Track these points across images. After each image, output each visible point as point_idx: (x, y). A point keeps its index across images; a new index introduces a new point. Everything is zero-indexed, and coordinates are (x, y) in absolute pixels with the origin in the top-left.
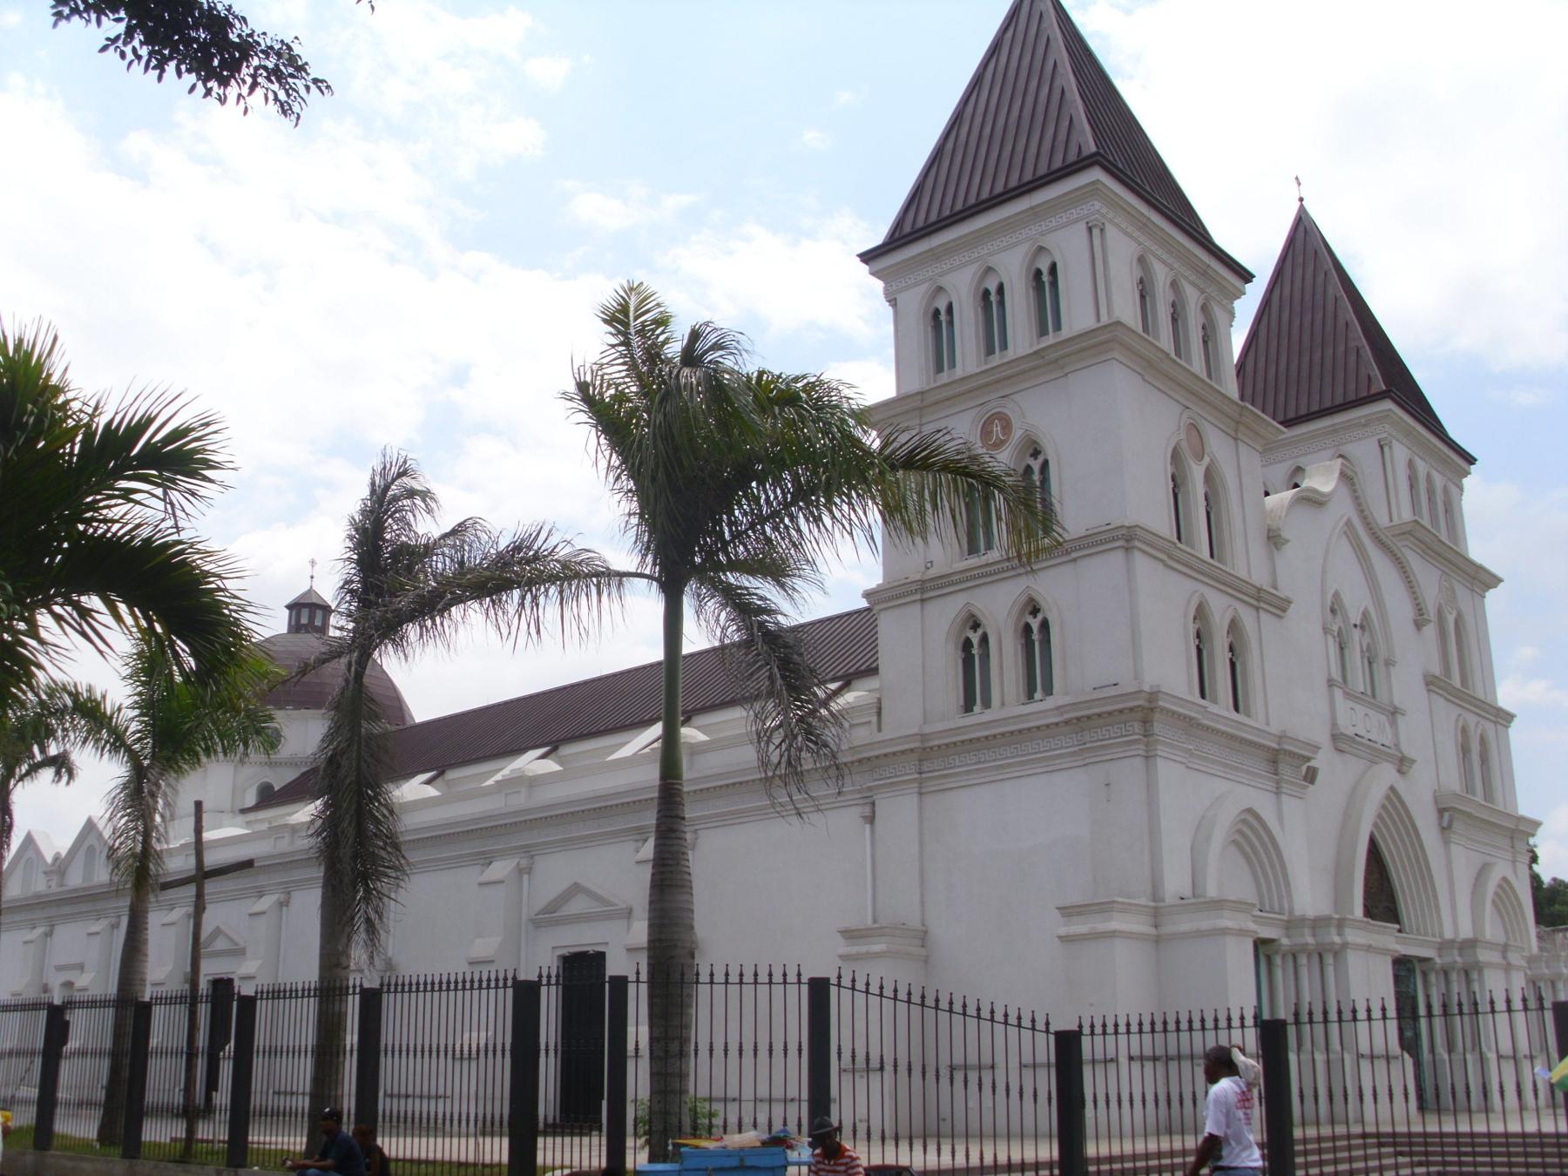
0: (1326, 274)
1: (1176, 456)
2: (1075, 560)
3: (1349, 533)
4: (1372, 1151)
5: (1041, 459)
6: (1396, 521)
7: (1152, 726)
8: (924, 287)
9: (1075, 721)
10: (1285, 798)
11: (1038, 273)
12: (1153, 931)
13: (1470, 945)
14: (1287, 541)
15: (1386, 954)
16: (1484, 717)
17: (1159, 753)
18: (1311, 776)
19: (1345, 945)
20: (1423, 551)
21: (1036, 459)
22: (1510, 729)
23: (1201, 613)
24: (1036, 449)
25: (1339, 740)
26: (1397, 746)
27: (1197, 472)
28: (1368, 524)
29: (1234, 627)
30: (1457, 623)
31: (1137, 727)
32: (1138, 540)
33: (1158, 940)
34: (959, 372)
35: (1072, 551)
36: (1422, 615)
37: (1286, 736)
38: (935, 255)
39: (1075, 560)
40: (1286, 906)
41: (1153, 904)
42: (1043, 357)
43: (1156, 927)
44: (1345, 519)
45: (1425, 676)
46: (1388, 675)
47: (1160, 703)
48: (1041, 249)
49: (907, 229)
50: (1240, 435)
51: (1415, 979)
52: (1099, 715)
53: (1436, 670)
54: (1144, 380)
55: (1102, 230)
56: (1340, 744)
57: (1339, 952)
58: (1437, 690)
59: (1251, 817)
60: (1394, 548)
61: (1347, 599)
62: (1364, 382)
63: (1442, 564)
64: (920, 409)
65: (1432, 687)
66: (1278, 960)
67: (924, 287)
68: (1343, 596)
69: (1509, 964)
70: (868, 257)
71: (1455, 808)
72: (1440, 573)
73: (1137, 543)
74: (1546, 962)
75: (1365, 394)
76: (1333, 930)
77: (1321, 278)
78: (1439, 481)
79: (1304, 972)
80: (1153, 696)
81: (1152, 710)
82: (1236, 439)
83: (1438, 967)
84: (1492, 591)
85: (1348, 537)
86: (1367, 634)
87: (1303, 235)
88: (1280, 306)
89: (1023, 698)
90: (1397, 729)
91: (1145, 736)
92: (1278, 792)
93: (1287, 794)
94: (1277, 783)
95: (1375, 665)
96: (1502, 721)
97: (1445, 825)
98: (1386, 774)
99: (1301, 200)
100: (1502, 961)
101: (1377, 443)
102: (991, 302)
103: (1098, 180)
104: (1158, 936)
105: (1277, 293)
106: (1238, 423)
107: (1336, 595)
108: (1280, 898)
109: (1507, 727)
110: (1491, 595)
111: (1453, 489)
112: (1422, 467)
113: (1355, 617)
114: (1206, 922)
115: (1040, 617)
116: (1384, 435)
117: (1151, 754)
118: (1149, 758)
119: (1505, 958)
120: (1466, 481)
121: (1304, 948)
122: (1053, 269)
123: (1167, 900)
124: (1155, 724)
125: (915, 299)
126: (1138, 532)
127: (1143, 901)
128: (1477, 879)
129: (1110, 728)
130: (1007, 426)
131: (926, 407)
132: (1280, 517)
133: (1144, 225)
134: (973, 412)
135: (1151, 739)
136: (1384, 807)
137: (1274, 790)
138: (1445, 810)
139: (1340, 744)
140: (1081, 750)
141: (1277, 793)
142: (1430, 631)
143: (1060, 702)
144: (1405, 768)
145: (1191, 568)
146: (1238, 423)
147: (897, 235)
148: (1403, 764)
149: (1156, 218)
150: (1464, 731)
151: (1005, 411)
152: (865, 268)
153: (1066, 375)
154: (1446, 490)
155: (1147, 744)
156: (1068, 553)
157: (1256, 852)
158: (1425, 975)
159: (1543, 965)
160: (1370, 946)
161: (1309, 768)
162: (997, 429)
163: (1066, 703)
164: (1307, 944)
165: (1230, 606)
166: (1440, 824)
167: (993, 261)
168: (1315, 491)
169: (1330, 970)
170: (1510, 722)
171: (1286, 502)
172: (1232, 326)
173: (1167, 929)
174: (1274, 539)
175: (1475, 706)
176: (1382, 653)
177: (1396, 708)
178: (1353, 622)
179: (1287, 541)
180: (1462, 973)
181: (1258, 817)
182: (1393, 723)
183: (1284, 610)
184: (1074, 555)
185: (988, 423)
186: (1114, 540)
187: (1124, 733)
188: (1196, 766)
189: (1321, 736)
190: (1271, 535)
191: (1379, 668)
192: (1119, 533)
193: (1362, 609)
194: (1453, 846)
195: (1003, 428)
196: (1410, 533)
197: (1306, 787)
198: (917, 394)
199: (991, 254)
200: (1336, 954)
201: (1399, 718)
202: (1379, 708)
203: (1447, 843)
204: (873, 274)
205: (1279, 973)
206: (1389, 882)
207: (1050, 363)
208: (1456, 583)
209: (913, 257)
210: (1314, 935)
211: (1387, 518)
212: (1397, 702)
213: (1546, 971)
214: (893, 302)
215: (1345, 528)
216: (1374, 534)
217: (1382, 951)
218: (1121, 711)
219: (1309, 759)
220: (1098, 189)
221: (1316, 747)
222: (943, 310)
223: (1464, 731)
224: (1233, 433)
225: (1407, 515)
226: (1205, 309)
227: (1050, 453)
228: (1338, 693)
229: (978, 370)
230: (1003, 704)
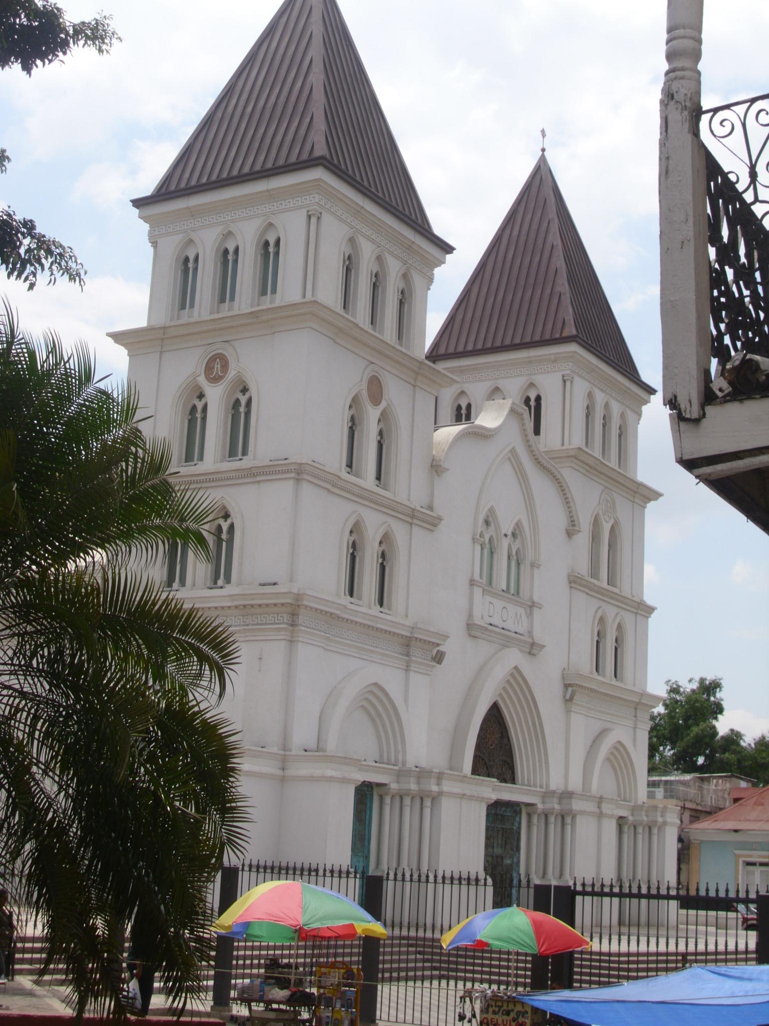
0: (549, 223)
1: (355, 402)
2: (259, 482)
4: (404, 949)
9: (242, 607)
10: (412, 674)
11: (267, 244)
12: (279, 772)
13: (567, 795)
14: (447, 470)
15: (481, 801)
16: (623, 608)
18: (439, 658)
19: (440, 794)
21: (244, 394)
22: (650, 619)
23: (356, 529)
24: (245, 387)
25: (472, 629)
26: (530, 633)
27: (372, 414)
29: (386, 539)
30: (613, 529)
31: (286, 618)
33: (283, 780)
37: (417, 628)
38: (192, 213)
39: (259, 482)
40: (400, 759)
41: (282, 752)
42: (257, 317)
43: (283, 769)
44: (510, 448)
45: (569, 576)
47: (305, 603)
48: (271, 225)
50: (418, 383)
51: (520, 819)
52: (260, 605)
53: (583, 569)
54: (334, 342)
56: (473, 632)
57: (436, 799)
58: (578, 587)
59: (376, 691)
65: (573, 585)
66: (388, 800)
69: (601, 813)
70: (138, 203)
71: (577, 685)
73: (306, 477)
74: (647, 811)
75: (558, 336)
76: (433, 781)
80: (299, 597)
81: (299, 606)
82: (414, 386)
83: (539, 811)
84: (652, 503)
85: (511, 462)
86: (518, 541)
87: (538, 183)
88: (508, 245)
89: (209, 583)
92: (407, 670)
95: (522, 567)
97: (568, 697)
98: (514, 657)
99: (543, 150)
100: (597, 810)
102: (228, 260)
105: (508, 232)
106: (417, 373)
107: (491, 510)
108: (396, 751)
109: (648, 617)
111: (630, 415)
112: (600, 398)
113: (507, 527)
116: (568, 372)
118: (291, 642)
119: (599, 807)
121: (408, 793)
122: (278, 242)
124: (301, 617)
125: (172, 244)
127: (274, 749)
128: (594, 741)
129: (267, 616)
130: (225, 366)
131: (166, 338)
132: (444, 451)
133: (358, 212)
135: (296, 628)
137: (405, 667)
138: (570, 685)
139: (473, 632)
140: (244, 629)
141: (406, 670)
142: (583, 539)
143: (232, 592)
144: (534, 651)
146: (417, 373)
147: (163, 191)
148: (532, 649)
149: (369, 206)
150: (602, 621)
151: (225, 353)
153: (274, 333)
154: (623, 416)
157: (379, 715)
158: (529, 816)
159: (644, 813)
160: (464, 795)
161: (438, 651)
162: (217, 366)
165: (385, 523)
168: (482, 428)
169: (427, 812)
170: (651, 613)
173: (291, 772)
174: (436, 468)
176: (530, 555)
177: (533, 602)
178: (504, 532)
179: (447, 470)
180: (560, 818)
181: (382, 690)
182: (530, 615)
183: (435, 526)
184: (258, 478)
186: (288, 472)
188: (334, 649)
190: (434, 463)
191: (525, 568)
192: (292, 467)
193: (515, 521)
194: (573, 715)
195: (222, 366)
196: (575, 457)
198: (161, 328)
199: (233, 221)
201: (536, 611)
203: (568, 712)
204: (140, 217)
205: (387, 809)
208: (615, 495)
209: (174, 211)
210: (418, 783)
211: (560, 443)
212: (536, 599)
213: (645, 818)
214: (154, 244)
215: (510, 455)
216: (536, 459)
217: (480, 799)
219: (438, 645)
220: (320, 185)
222: (191, 259)
223: (602, 621)
224: (412, 382)
225: (577, 440)
226: (405, 276)
227: (253, 392)
228: (478, 591)
230: (194, 585)
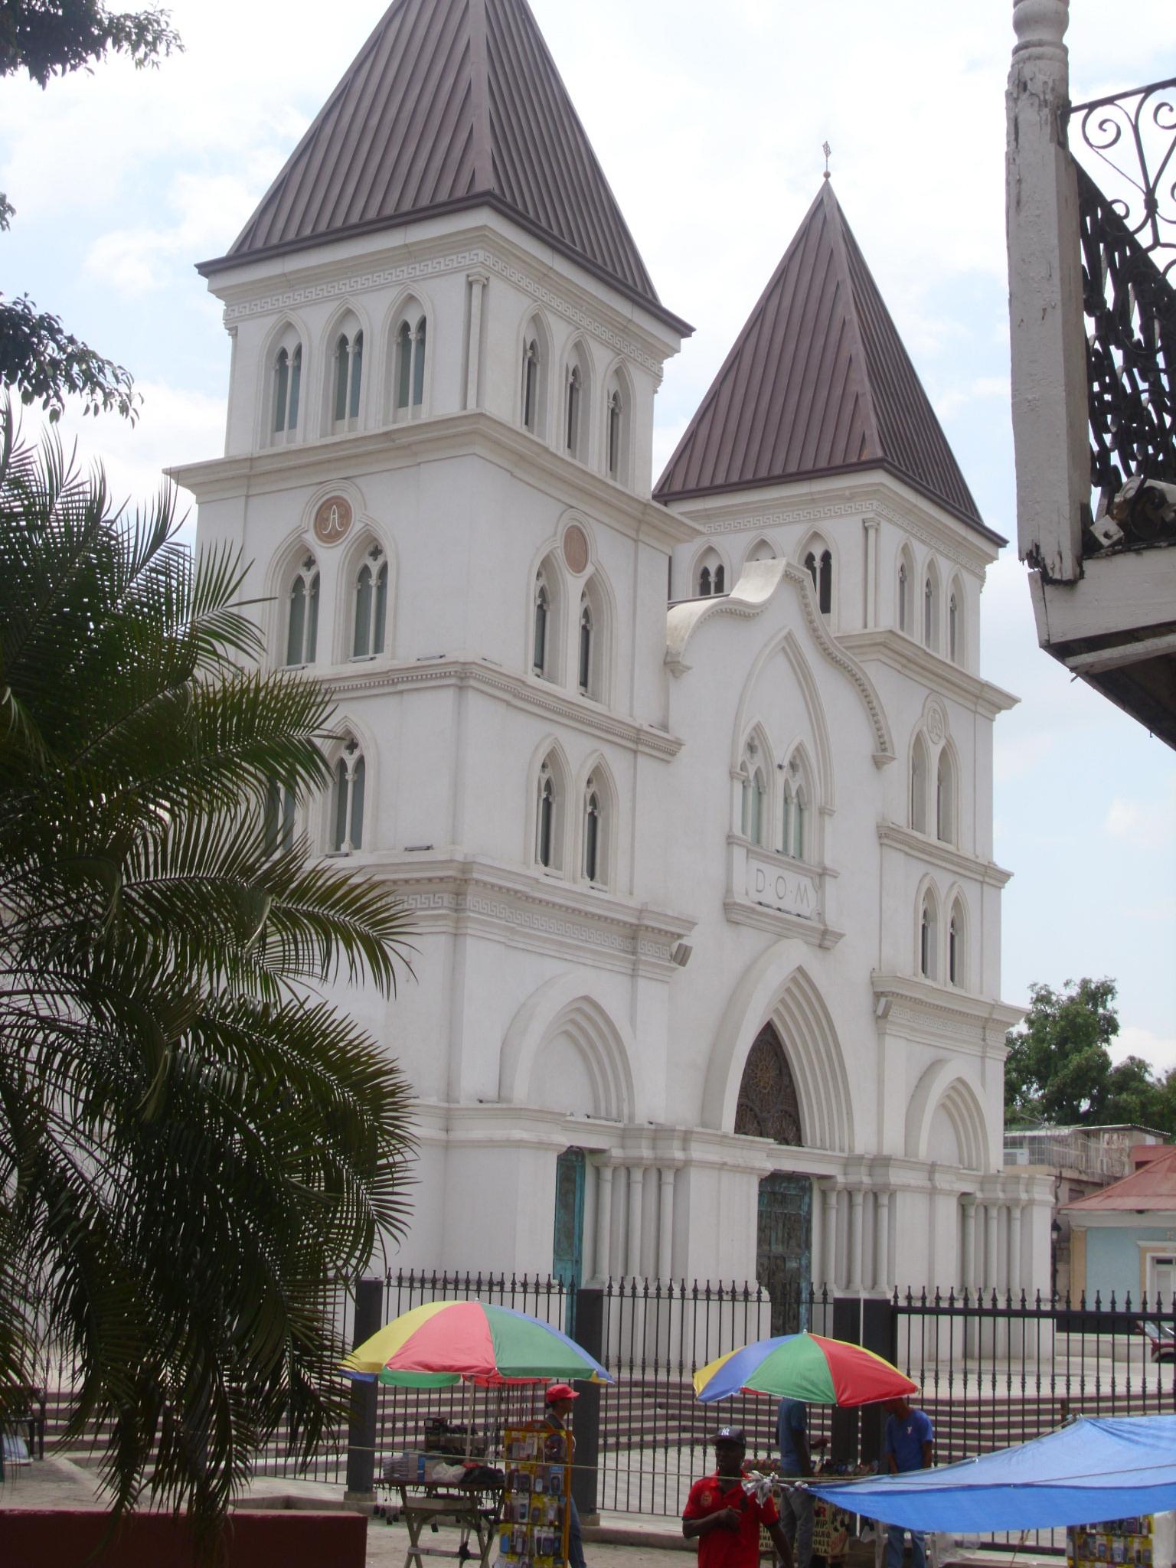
1: (546, 568)
2: (401, 692)
3: (787, 647)
4: (637, 1401)
5: (380, 560)
6: (871, 628)
7: (465, 899)
8: (273, 318)
10: (642, 983)
11: (406, 327)
12: (442, 1135)
13: (881, 1162)
14: (689, 668)
15: (750, 1173)
17: (469, 931)
18: (682, 956)
19: (688, 1163)
20: (904, 666)
23: (551, 761)
24: (376, 547)
25: (732, 912)
27: (572, 586)
28: (818, 638)
29: (597, 776)
30: (944, 754)
31: (447, 899)
32: (475, 678)
34: (299, 443)
35: (398, 682)
36: (884, 750)
38: (289, 282)
39: (401, 692)
40: (626, 1111)
41: (445, 1105)
42: (393, 441)
43: (447, 1131)
46: (822, 829)
47: (475, 875)
49: (259, 244)
51: (811, 1198)
53: (900, 817)
55: (484, 286)
57: (680, 1170)
60: (852, 666)
61: (771, 733)
62: (856, 443)
63: (930, 680)
64: (248, 477)
65: (885, 841)
67: (273, 318)
68: (767, 730)
70: (207, 269)
72: (927, 692)
73: (472, 682)
74: (1003, 1184)
76: (677, 1144)
77: (832, 289)
78: (946, 569)
79: (637, 1189)
80: (466, 867)
81: (466, 880)
82: (636, 541)
83: (839, 1187)
87: (820, 226)
90: (823, 893)
91: (456, 910)
92: (634, 975)
93: (645, 977)
94: (634, 964)
95: (806, 814)
96: (992, 882)
97: (880, 1012)
98: (796, 953)
99: (827, 175)
101: (860, 524)
102: (348, 354)
103: (486, 226)
104: (448, 1142)
105: (775, 301)
106: (640, 521)
107: (758, 729)
108: (619, 1099)
110: (1002, 718)
111: (967, 578)
112: (921, 554)
113: (782, 754)
114: (499, 1131)
115: (357, 753)
116: (871, 515)
117: (460, 931)
118: (456, 935)
120: (990, 569)
121: (638, 1162)
123: (462, 1102)
124: (469, 898)
125: (260, 331)
126: (475, 670)
129: (418, 897)
130: (346, 515)
132: (683, 639)
133: (545, 276)
134: (314, 489)
135: (462, 915)
136: (788, 990)
141: (632, 976)
142: (899, 769)
144: (827, 943)
145: (548, 709)
146: (640, 521)
147: (245, 249)
148: (825, 939)
150: (930, 894)
152: (204, 282)
153: (419, 464)
155: (458, 921)
156: (394, 683)
158: (824, 1194)
159: (999, 1187)
160: (725, 1164)
162: (334, 517)
163: (370, 863)
164: (642, 1158)
166: (875, 1012)
167: (354, 303)
168: (741, 602)
169: (668, 1191)
171: (695, 619)
172: (656, 392)
173: (459, 1134)
174: (672, 666)
175: (952, 863)
176: (818, 796)
177: (825, 869)
178: (777, 762)
179: (689, 668)
182: (820, 888)
183: (673, 754)
184: (400, 687)
185: (326, 506)
186: (445, 676)
187: (432, 905)
188: (521, 946)
189: (705, 910)
190: (669, 659)
192: (452, 669)
195: (341, 517)
197: (674, 969)
198: (246, 460)
200: (678, 1172)
202: (805, 872)
203: (881, 1034)
205: (607, 1188)
206: (791, 1080)
207: (403, 447)
208: (947, 702)
212: (828, 863)
213: (1001, 1195)
214: (233, 331)
217: (749, 1170)
218: (430, 880)
219: (680, 936)
220: (485, 236)
221: (689, 922)
222: (291, 353)
223: (930, 894)
225: (888, 619)
226: (619, 373)
227: (389, 554)
228: (739, 853)
229: (318, 444)
